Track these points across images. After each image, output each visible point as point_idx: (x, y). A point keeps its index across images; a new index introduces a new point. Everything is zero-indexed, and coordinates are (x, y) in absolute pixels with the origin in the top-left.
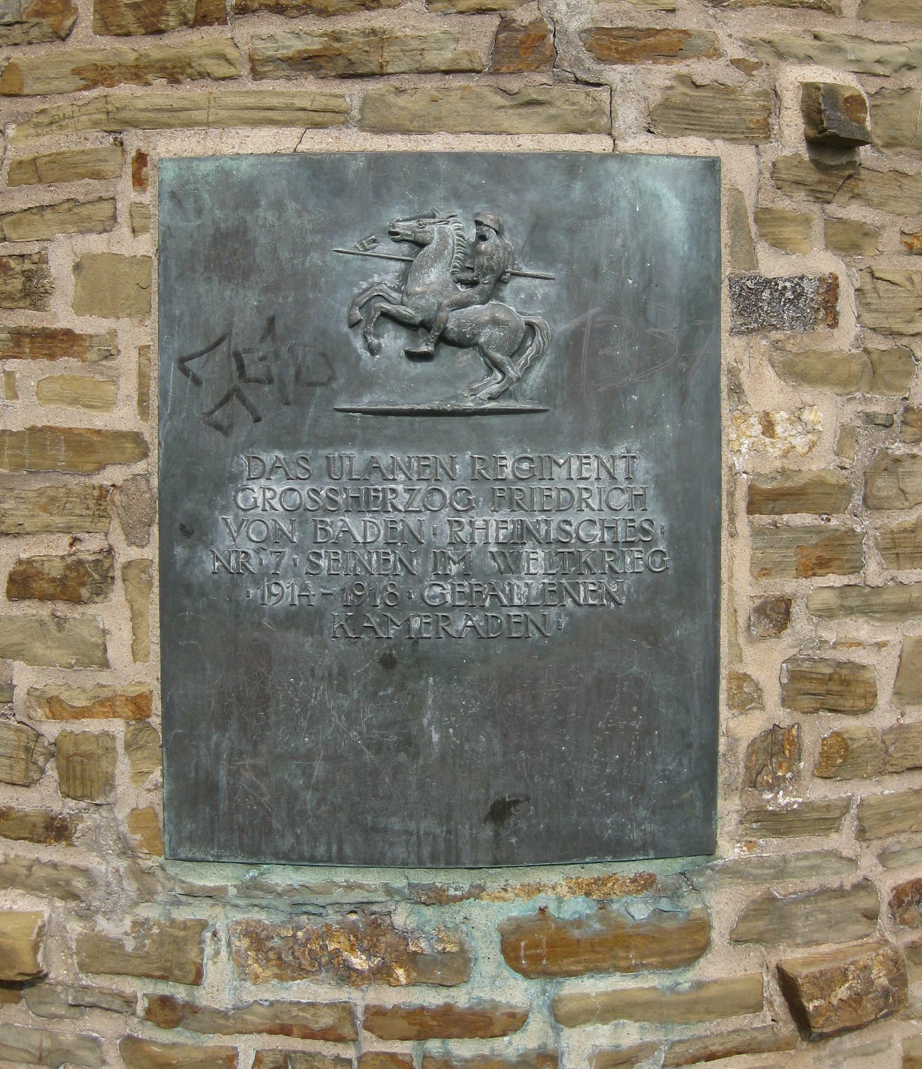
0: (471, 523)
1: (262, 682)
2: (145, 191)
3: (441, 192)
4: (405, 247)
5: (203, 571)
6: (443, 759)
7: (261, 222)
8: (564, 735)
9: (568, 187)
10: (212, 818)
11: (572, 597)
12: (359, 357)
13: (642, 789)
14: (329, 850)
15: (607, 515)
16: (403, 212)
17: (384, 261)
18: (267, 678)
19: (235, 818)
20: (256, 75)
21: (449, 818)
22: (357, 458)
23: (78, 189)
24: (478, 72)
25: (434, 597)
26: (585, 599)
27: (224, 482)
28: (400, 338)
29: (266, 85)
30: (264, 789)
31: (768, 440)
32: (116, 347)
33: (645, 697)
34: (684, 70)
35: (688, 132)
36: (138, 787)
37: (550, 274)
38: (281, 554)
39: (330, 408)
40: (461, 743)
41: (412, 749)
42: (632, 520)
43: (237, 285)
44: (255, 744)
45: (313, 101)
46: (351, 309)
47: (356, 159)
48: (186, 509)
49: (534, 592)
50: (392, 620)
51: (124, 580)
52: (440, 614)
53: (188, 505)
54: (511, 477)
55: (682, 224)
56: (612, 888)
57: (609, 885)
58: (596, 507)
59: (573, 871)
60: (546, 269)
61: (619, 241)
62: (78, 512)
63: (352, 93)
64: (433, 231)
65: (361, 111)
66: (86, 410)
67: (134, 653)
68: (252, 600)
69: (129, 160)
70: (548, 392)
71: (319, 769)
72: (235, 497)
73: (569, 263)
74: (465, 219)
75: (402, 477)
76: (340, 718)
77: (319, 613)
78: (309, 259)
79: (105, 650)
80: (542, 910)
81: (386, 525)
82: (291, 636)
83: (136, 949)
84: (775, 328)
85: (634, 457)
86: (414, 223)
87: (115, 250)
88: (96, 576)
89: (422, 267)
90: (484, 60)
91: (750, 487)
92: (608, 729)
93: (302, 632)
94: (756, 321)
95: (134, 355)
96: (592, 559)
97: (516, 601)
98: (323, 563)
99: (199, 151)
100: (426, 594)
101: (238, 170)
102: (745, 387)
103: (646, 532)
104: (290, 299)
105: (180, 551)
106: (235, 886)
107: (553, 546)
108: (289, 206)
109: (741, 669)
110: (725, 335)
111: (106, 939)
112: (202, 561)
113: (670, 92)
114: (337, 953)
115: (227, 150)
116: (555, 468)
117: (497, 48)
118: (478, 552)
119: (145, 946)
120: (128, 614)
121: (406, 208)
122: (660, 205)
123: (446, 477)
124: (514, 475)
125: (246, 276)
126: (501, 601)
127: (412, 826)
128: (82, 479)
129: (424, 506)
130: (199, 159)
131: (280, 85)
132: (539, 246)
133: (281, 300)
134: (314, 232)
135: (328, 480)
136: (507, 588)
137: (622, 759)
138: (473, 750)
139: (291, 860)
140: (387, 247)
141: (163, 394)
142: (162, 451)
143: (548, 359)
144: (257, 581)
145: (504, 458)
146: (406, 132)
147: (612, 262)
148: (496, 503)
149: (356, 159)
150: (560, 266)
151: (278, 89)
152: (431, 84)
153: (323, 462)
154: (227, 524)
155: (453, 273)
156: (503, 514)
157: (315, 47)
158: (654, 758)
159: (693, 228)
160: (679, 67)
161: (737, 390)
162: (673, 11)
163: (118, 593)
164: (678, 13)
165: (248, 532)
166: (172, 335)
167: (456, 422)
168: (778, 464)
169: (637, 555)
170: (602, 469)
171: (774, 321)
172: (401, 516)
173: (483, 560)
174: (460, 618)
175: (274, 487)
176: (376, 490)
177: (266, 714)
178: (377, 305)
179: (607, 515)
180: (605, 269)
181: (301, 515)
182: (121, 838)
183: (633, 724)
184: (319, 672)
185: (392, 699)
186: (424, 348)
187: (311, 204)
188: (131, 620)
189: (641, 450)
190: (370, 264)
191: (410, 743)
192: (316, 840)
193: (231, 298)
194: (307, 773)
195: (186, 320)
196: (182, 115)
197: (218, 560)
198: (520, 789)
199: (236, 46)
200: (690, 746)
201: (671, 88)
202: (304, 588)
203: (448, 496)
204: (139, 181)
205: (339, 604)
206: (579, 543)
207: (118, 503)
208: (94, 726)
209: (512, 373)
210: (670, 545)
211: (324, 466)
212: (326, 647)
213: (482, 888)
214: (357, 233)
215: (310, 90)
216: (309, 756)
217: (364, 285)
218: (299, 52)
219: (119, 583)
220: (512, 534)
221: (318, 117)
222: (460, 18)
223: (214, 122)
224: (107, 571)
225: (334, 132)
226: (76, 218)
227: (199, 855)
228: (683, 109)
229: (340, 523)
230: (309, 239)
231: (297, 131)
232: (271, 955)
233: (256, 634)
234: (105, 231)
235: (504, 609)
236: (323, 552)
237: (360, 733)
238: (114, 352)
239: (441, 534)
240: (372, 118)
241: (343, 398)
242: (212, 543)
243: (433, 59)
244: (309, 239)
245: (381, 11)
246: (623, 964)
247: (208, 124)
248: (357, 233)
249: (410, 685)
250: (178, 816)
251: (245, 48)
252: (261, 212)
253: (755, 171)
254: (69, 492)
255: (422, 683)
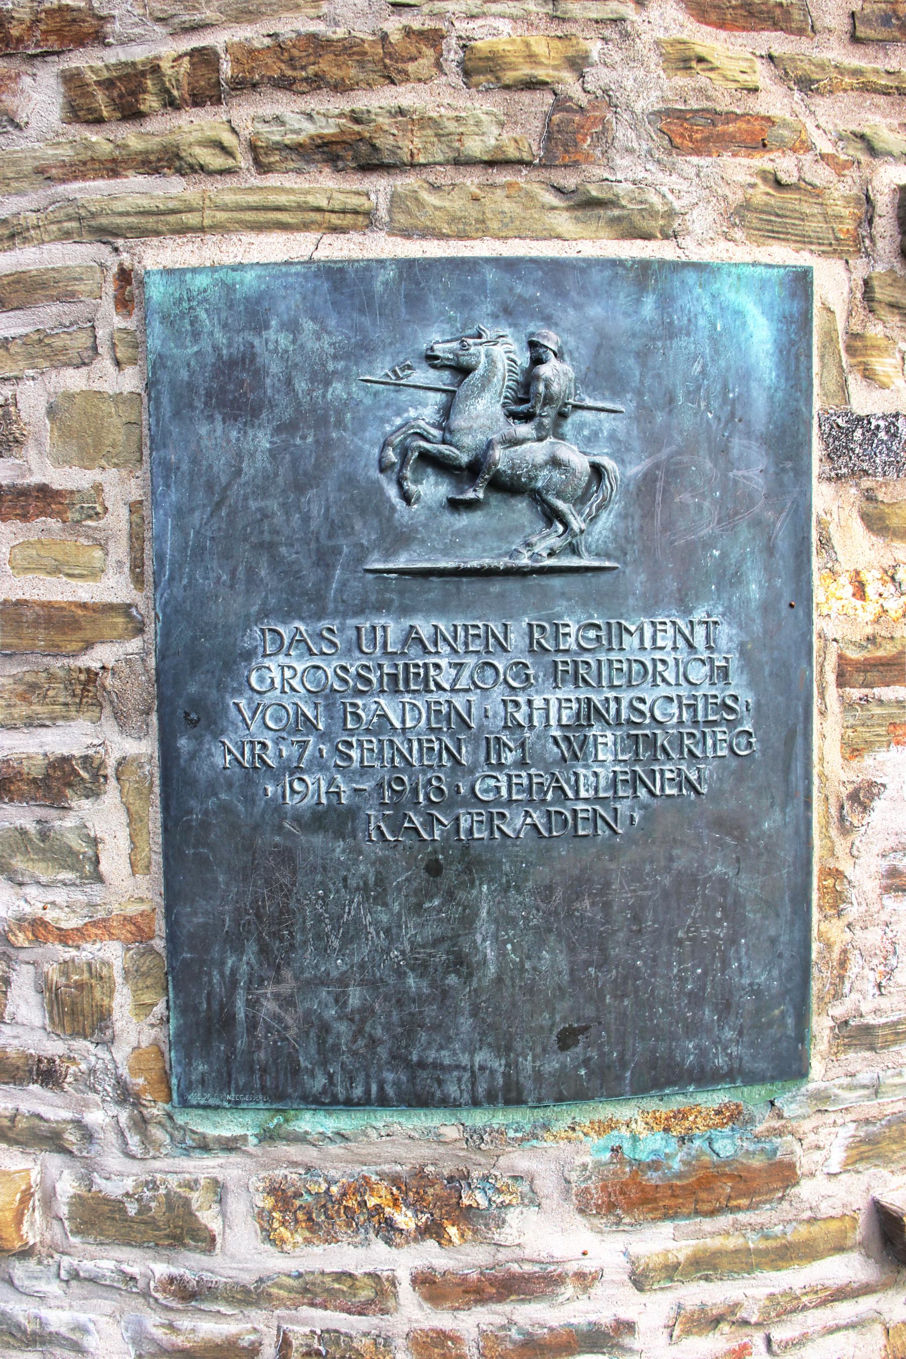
0: (530, 703)
1: (285, 896)
2: (130, 315)
3: (488, 307)
4: (446, 375)
5: (213, 766)
6: (499, 980)
7: (271, 346)
8: (639, 948)
9: (638, 301)
10: (228, 1058)
11: (646, 786)
12: (393, 508)
13: (728, 1006)
14: (368, 1092)
15: (684, 691)
16: (443, 333)
17: (421, 392)
18: (290, 891)
19: (255, 1057)
20: (263, 168)
21: (509, 1049)
22: (393, 629)
23: (48, 314)
24: (528, 164)
25: (486, 791)
26: (662, 789)
27: (233, 662)
28: (442, 484)
29: (273, 180)
30: (290, 1022)
31: (859, 603)
32: (103, 504)
33: (730, 900)
34: (769, 167)
35: (770, 241)
36: (136, 1026)
37: (618, 407)
38: (304, 745)
39: (360, 569)
40: (521, 961)
41: (464, 970)
42: (715, 697)
43: (245, 424)
44: (278, 968)
45: (329, 199)
46: (383, 449)
47: (384, 268)
48: (188, 692)
49: (602, 783)
50: (438, 820)
51: (118, 779)
52: (494, 811)
53: (193, 689)
54: (574, 647)
55: (769, 347)
56: (694, 1122)
57: (691, 1118)
58: (673, 682)
59: (651, 1104)
60: (612, 400)
61: (697, 368)
62: (62, 700)
63: (379, 189)
64: (478, 352)
65: (390, 211)
66: (69, 580)
67: (132, 865)
68: (272, 799)
69: (110, 279)
70: (620, 546)
71: (355, 997)
72: (248, 678)
73: (639, 393)
74: (517, 340)
75: (444, 649)
76: (378, 934)
77: (352, 813)
78: (331, 390)
79: (98, 862)
80: (616, 1150)
81: (429, 708)
82: (318, 840)
83: (140, 1212)
84: (866, 473)
85: (715, 623)
86: (455, 345)
87: (96, 386)
88: (85, 775)
89: (467, 397)
90: (535, 148)
91: (841, 657)
92: (690, 939)
93: (331, 835)
94: (846, 466)
95: (124, 512)
96: (669, 742)
97: (583, 794)
98: (355, 754)
99: (194, 262)
100: (477, 787)
101: (242, 283)
102: (834, 541)
103: (731, 710)
104: (310, 440)
105: (183, 743)
106: (256, 1136)
107: (625, 728)
108: (305, 326)
109: (832, 864)
110: (814, 480)
111: (106, 1200)
112: (210, 754)
113: (750, 191)
114: (378, 1208)
115: (228, 260)
116: (625, 636)
117: (550, 136)
118: (538, 737)
119: (150, 1209)
120: (124, 819)
121: (446, 326)
122: (744, 324)
123: (499, 649)
124: (579, 645)
125: (255, 412)
126: (565, 794)
127: (464, 1059)
128: (66, 661)
129: (474, 683)
130: (194, 270)
131: (290, 181)
132: (602, 375)
133: (298, 441)
134: (335, 357)
135: (357, 654)
136: (573, 779)
137: (705, 973)
138: (535, 969)
139: (323, 1104)
140: (423, 375)
141: (160, 558)
142: (159, 625)
143: (616, 507)
144: (275, 775)
145: (567, 625)
146: (442, 236)
147: (689, 393)
148: (556, 676)
149: (384, 268)
150: (629, 396)
151: (287, 185)
152: (472, 180)
153: (352, 634)
154: (240, 711)
155: (504, 405)
156: (567, 692)
157: (331, 131)
158: (740, 970)
159: (781, 352)
160: (761, 161)
161: (825, 543)
162: (756, 90)
163: (111, 795)
164: (761, 95)
165: (264, 718)
166: (168, 486)
167: (512, 585)
168: (869, 630)
169: (720, 736)
170: (679, 637)
171: (865, 466)
172: (446, 696)
173: (544, 746)
174: (518, 814)
175: (295, 665)
176: (416, 666)
177: (291, 933)
178: (415, 444)
179: (684, 691)
180: (681, 400)
181: (326, 697)
182: (120, 1083)
183: (717, 931)
184: (352, 883)
185: (440, 911)
186: (470, 495)
187: (332, 323)
188: (129, 825)
189: (723, 615)
190: (404, 396)
191: (460, 963)
192: (352, 1080)
193: (238, 439)
194: (340, 1000)
195: (185, 467)
196: (171, 219)
197: (230, 752)
198: (589, 1011)
199: (234, 131)
200: (780, 956)
201: (753, 186)
202: (331, 782)
203: (501, 671)
204: (124, 303)
205: (374, 802)
206: (654, 724)
207: (109, 688)
208: (88, 952)
209: (577, 523)
210: (756, 725)
211: (354, 638)
212: (360, 853)
213: (546, 1127)
214: (388, 358)
215: (325, 186)
216: (343, 981)
217: (398, 421)
218: (312, 138)
219: (112, 782)
220: (578, 714)
221: (335, 219)
222: (507, 95)
223: (211, 227)
224: (99, 769)
225: (355, 236)
226: (48, 350)
227: (212, 1102)
228: (763, 212)
229: (374, 706)
230: (331, 366)
231: (312, 237)
232: (300, 1215)
233: (277, 839)
234: (84, 364)
235: (568, 803)
236: (354, 740)
237: (403, 953)
238: (99, 509)
239: (495, 716)
240: (402, 219)
241: (376, 556)
242: (223, 732)
243: (475, 147)
244: (331, 366)
245: (409, 86)
246: (706, 1207)
247: (202, 229)
248: (388, 358)
249: (461, 895)
250: (188, 1056)
251: (245, 133)
252: (271, 334)
253: (846, 290)
254: (51, 677)
255: (475, 892)
